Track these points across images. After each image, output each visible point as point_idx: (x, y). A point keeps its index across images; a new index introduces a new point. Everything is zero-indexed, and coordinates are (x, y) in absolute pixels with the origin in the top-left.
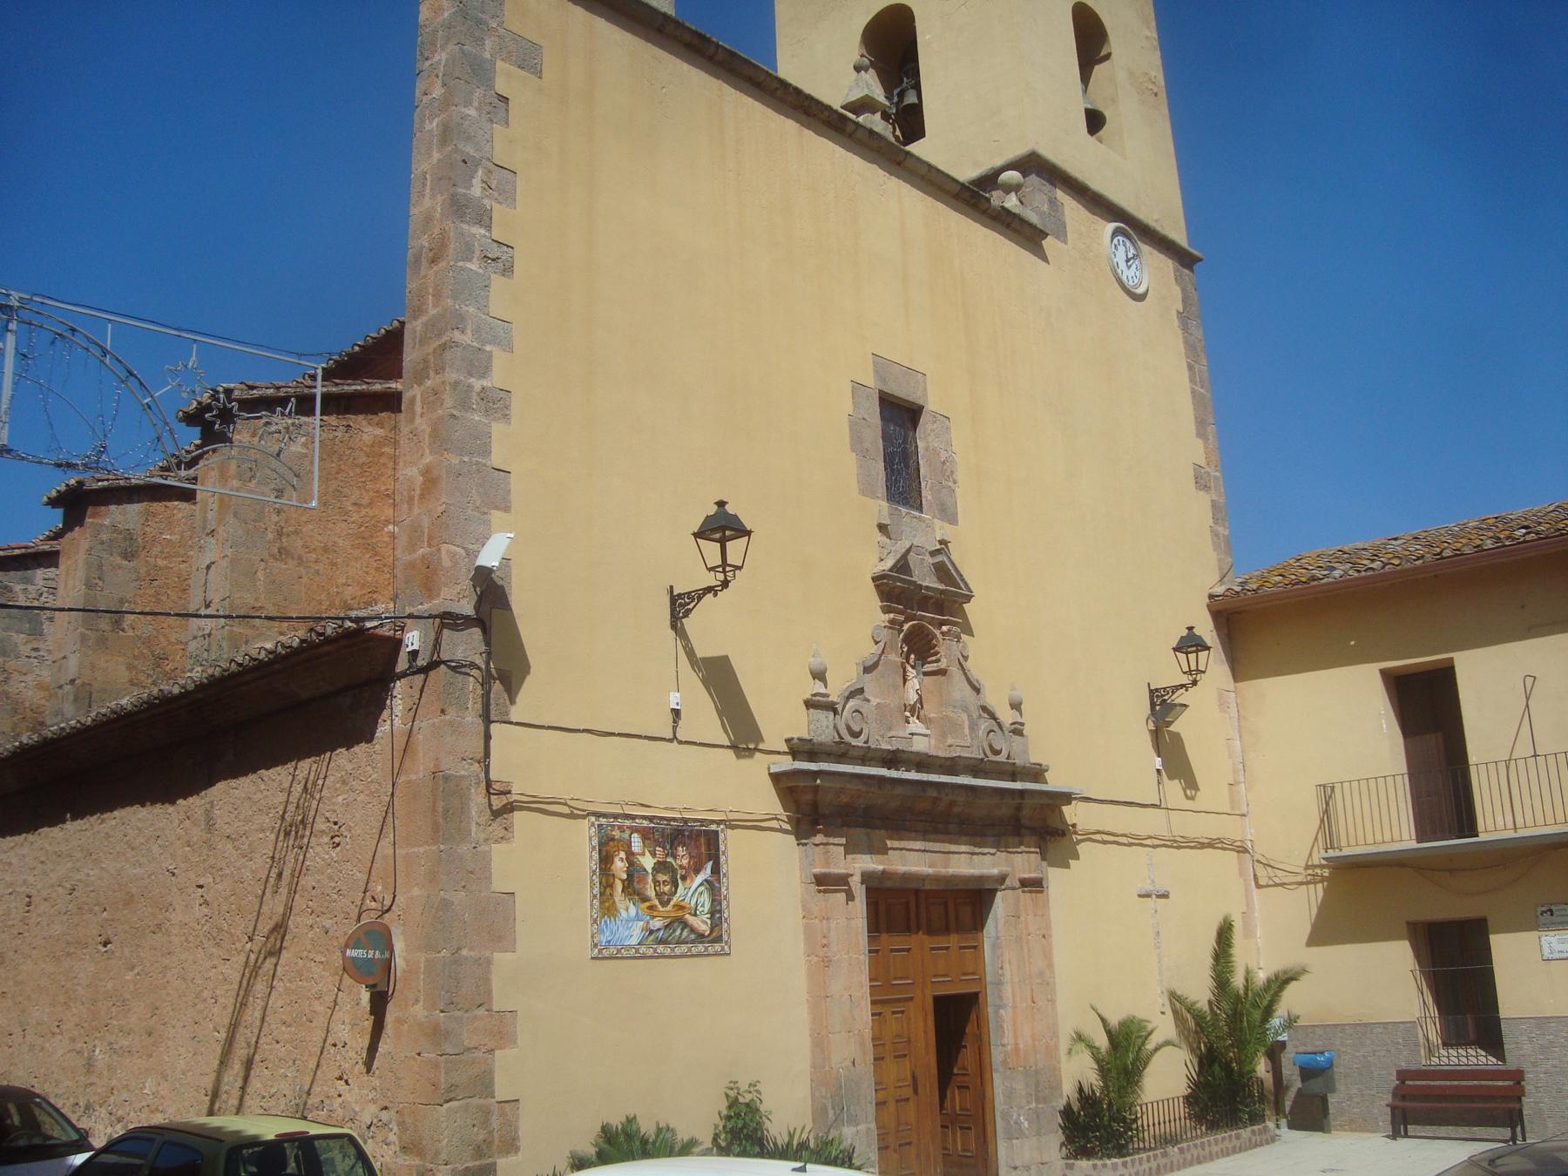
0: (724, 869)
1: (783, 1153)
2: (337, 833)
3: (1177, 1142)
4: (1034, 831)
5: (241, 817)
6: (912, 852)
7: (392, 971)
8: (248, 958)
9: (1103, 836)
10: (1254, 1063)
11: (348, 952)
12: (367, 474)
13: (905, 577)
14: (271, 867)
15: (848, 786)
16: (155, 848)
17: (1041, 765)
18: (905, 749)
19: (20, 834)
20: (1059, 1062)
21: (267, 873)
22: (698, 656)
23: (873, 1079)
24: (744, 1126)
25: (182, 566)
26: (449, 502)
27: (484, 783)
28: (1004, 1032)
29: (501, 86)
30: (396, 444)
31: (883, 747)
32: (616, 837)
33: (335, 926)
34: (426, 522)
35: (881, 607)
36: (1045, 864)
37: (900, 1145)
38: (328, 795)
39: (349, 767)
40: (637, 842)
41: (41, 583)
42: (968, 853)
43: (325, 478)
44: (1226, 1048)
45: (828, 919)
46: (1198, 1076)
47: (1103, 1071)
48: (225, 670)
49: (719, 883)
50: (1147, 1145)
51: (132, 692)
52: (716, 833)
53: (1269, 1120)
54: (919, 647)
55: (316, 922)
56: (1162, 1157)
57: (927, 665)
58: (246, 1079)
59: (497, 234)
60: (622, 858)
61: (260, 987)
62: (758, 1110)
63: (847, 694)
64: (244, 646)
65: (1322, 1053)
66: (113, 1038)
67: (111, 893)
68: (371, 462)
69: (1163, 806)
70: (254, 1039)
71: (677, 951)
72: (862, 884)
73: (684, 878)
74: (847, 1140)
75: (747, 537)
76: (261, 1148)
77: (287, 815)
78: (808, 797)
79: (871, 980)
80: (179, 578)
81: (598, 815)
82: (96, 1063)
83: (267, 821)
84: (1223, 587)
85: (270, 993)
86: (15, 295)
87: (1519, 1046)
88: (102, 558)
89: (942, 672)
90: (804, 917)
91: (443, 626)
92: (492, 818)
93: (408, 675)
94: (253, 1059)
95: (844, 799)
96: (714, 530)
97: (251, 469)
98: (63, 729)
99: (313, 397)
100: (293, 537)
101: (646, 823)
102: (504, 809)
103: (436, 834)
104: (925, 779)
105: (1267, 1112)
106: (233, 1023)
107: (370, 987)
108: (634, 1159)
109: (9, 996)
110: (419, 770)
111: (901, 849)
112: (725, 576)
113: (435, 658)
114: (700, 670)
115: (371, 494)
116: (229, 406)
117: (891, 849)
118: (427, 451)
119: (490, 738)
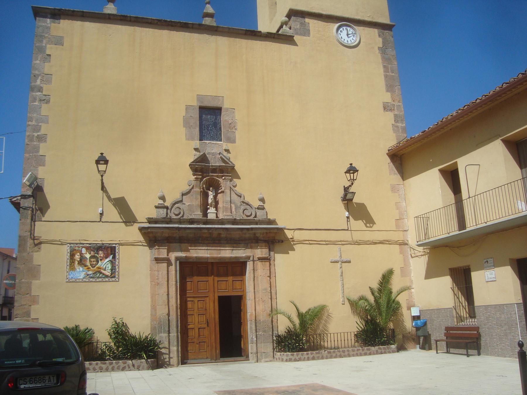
22: (112, 198)
29: (48, 52)
40: (84, 251)
42: (232, 250)
49: (115, 261)
52: (115, 247)
59: (44, 93)
69: (349, 229)
71: (97, 280)
73: (101, 260)
81: (70, 244)
87: (480, 317)
101: (88, 245)
102: (38, 244)
114: (112, 201)
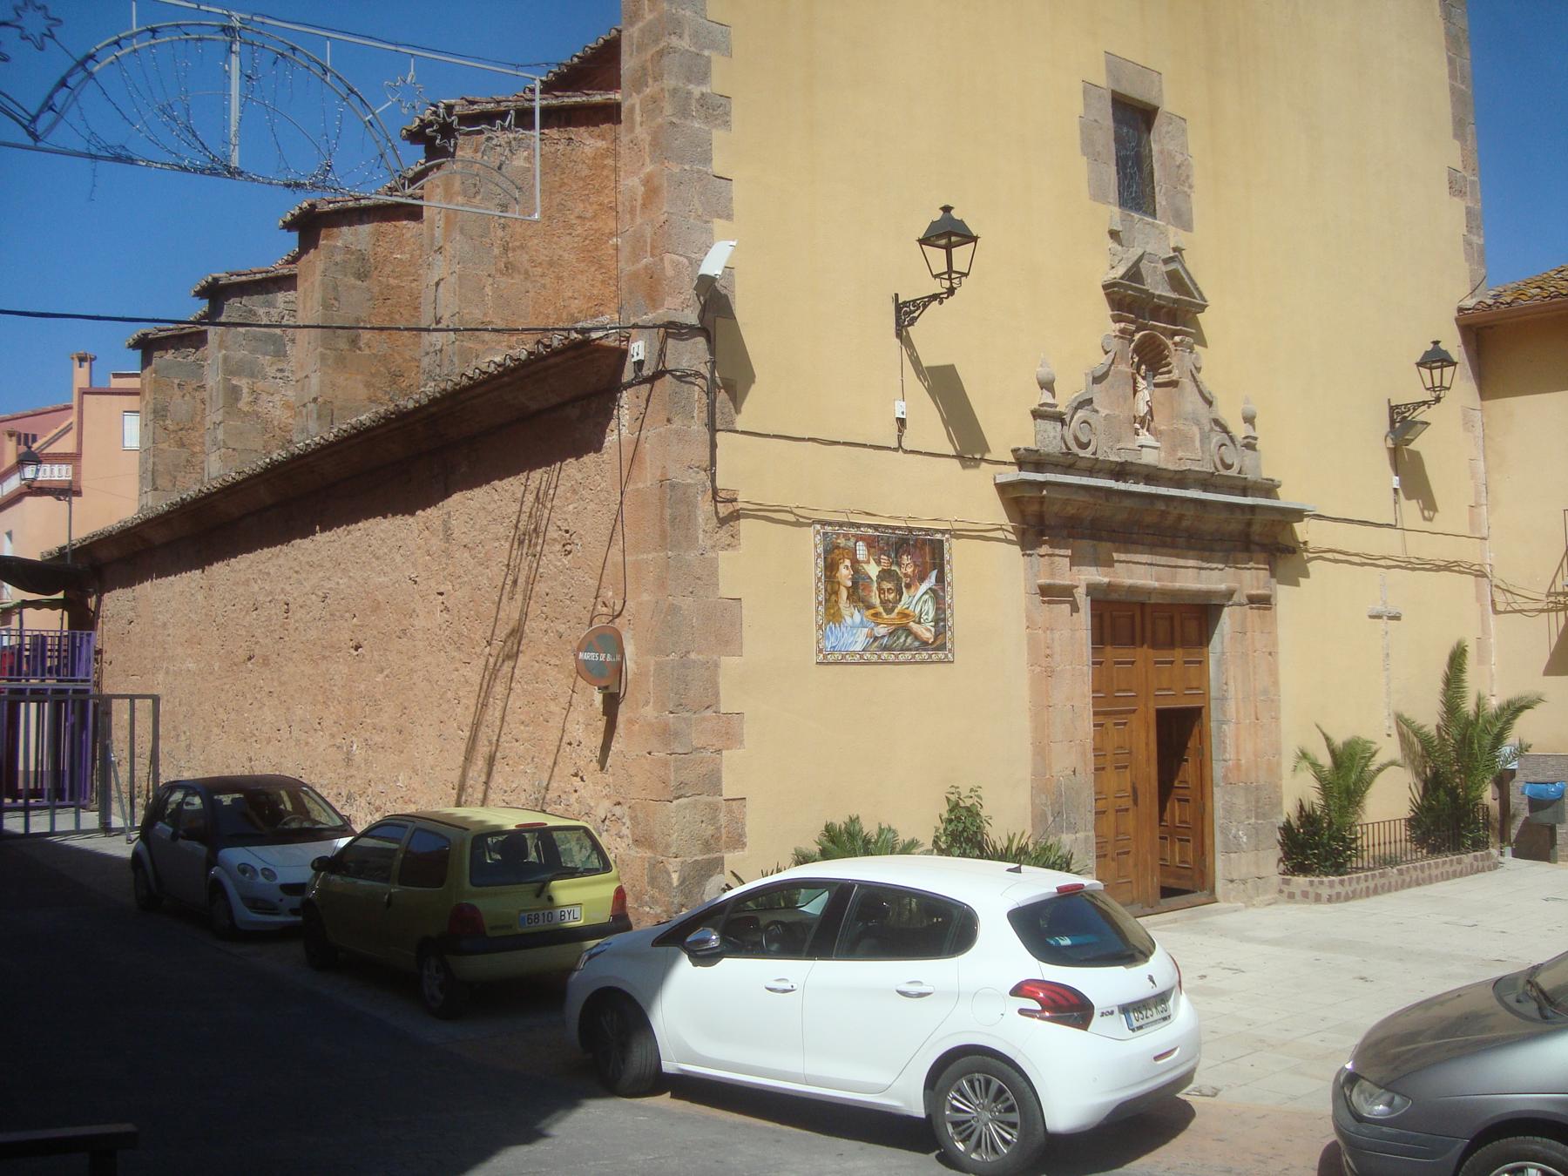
0: (948, 578)
1: (1002, 856)
2: (568, 541)
3: (1397, 864)
4: (1264, 547)
5: (477, 527)
6: (1138, 566)
7: (623, 674)
8: (487, 662)
9: (1335, 554)
10: (1480, 790)
11: (581, 655)
12: (590, 186)
13: (1137, 285)
14: (506, 575)
15: (1074, 497)
16: (398, 558)
17: (1272, 480)
18: (1134, 461)
19: (275, 546)
20: (1281, 780)
21: (503, 580)
22: (924, 366)
23: (1093, 789)
24: (964, 830)
25: (413, 285)
26: (672, 211)
27: (711, 491)
28: (1225, 748)
30: (616, 155)
31: (1111, 459)
32: (841, 545)
33: (568, 630)
34: (648, 232)
35: (1112, 316)
36: (1274, 581)
37: (1118, 854)
38: (559, 504)
39: (579, 476)
40: (862, 551)
41: (282, 306)
42: (1197, 568)
43: (548, 192)
44: (1452, 773)
45: (1052, 629)
46: (1422, 800)
47: (1326, 789)
48: (456, 384)
50: (1366, 864)
51: (371, 409)
53: (1493, 847)
54: (1151, 357)
55: (551, 627)
56: (1380, 877)
57: (1159, 376)
58: (489, 774)
60: (847, 566)
61: (499, 688)
62: (978, 814)
63: (1075, 404)
65: (1554, 783)
66: (367, 735)
67: (359, 600)
68: (593, 174)
70: (495, 738)
72: (1087, 595)
73: (908, 586)
74: (1065, 847)
75: (973, 243)
76: (505, 837)
77: (520, 524)
78: (1035, 508)
79: (1093, 692)
80: (410, 296)
81: (824, 523)
82: (354, 758)
83: (502, 530)
84: (1474, 300)
85: (509, 694)
86: (236, 15)
88: (337, 278)
89: (1173, 384)
90: (1028, 627)
91: (667, 335)
92: (718, 525)
93: (635, 385)
94: (494, 757)
95: (1071, 510)
96: (940, 236)
97: (475, 185)
98: (307, 445)
99: (532, 111)
100: (519, 252)
101: (870, 532)
103: (664, 542)
104: (1154, 492)
105: (1492, 840)
106: (475, 722)
107: (602, 688)
108: (856, 856)
109: (275, 695)
110: (646, 480)
111: (1128, 562)
112: (951, 283)
113: (660, 368)
114: (926, 379)
115: (595, 207)
116: (449, 120)
117: (1117, 561)
118: (648, 160)
119: (716, 446)
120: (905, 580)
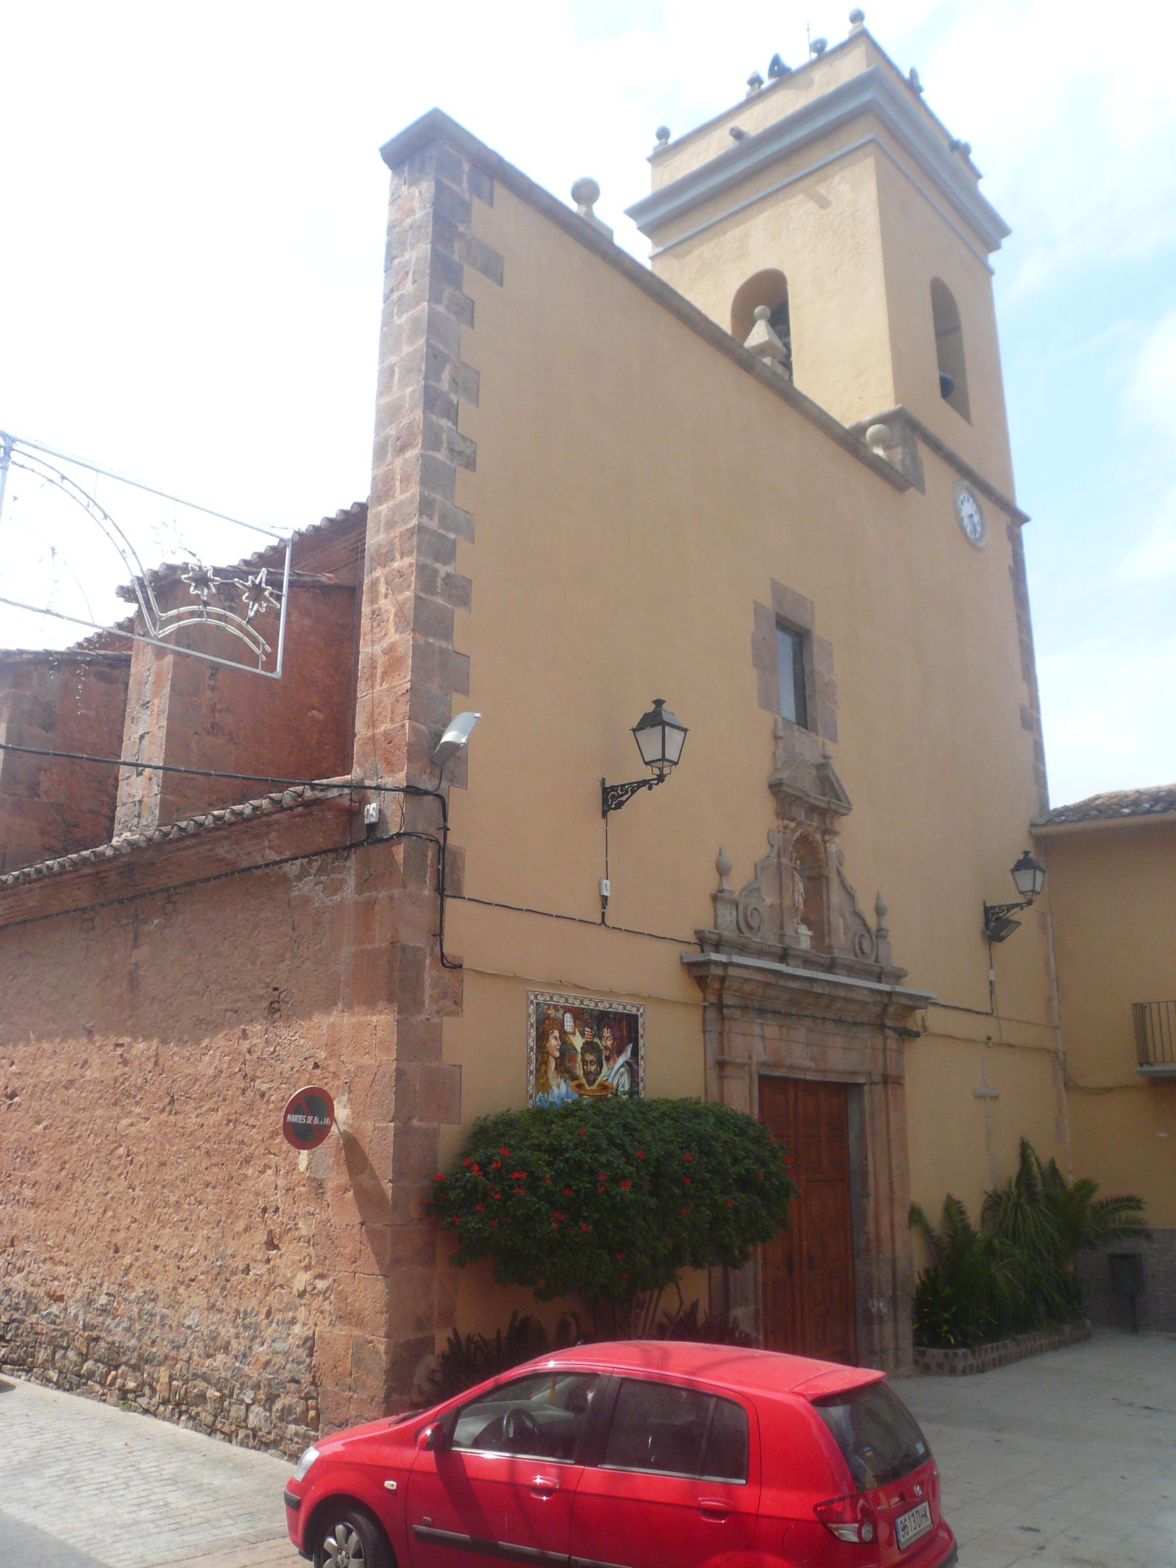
0: (642, 1052)
11: (289, 1117)
49: (638, 1065)
64: (175, 814)
73: (608, 1059)
118: (392, 630)
120: (605, 1053)
